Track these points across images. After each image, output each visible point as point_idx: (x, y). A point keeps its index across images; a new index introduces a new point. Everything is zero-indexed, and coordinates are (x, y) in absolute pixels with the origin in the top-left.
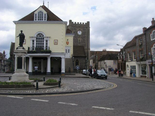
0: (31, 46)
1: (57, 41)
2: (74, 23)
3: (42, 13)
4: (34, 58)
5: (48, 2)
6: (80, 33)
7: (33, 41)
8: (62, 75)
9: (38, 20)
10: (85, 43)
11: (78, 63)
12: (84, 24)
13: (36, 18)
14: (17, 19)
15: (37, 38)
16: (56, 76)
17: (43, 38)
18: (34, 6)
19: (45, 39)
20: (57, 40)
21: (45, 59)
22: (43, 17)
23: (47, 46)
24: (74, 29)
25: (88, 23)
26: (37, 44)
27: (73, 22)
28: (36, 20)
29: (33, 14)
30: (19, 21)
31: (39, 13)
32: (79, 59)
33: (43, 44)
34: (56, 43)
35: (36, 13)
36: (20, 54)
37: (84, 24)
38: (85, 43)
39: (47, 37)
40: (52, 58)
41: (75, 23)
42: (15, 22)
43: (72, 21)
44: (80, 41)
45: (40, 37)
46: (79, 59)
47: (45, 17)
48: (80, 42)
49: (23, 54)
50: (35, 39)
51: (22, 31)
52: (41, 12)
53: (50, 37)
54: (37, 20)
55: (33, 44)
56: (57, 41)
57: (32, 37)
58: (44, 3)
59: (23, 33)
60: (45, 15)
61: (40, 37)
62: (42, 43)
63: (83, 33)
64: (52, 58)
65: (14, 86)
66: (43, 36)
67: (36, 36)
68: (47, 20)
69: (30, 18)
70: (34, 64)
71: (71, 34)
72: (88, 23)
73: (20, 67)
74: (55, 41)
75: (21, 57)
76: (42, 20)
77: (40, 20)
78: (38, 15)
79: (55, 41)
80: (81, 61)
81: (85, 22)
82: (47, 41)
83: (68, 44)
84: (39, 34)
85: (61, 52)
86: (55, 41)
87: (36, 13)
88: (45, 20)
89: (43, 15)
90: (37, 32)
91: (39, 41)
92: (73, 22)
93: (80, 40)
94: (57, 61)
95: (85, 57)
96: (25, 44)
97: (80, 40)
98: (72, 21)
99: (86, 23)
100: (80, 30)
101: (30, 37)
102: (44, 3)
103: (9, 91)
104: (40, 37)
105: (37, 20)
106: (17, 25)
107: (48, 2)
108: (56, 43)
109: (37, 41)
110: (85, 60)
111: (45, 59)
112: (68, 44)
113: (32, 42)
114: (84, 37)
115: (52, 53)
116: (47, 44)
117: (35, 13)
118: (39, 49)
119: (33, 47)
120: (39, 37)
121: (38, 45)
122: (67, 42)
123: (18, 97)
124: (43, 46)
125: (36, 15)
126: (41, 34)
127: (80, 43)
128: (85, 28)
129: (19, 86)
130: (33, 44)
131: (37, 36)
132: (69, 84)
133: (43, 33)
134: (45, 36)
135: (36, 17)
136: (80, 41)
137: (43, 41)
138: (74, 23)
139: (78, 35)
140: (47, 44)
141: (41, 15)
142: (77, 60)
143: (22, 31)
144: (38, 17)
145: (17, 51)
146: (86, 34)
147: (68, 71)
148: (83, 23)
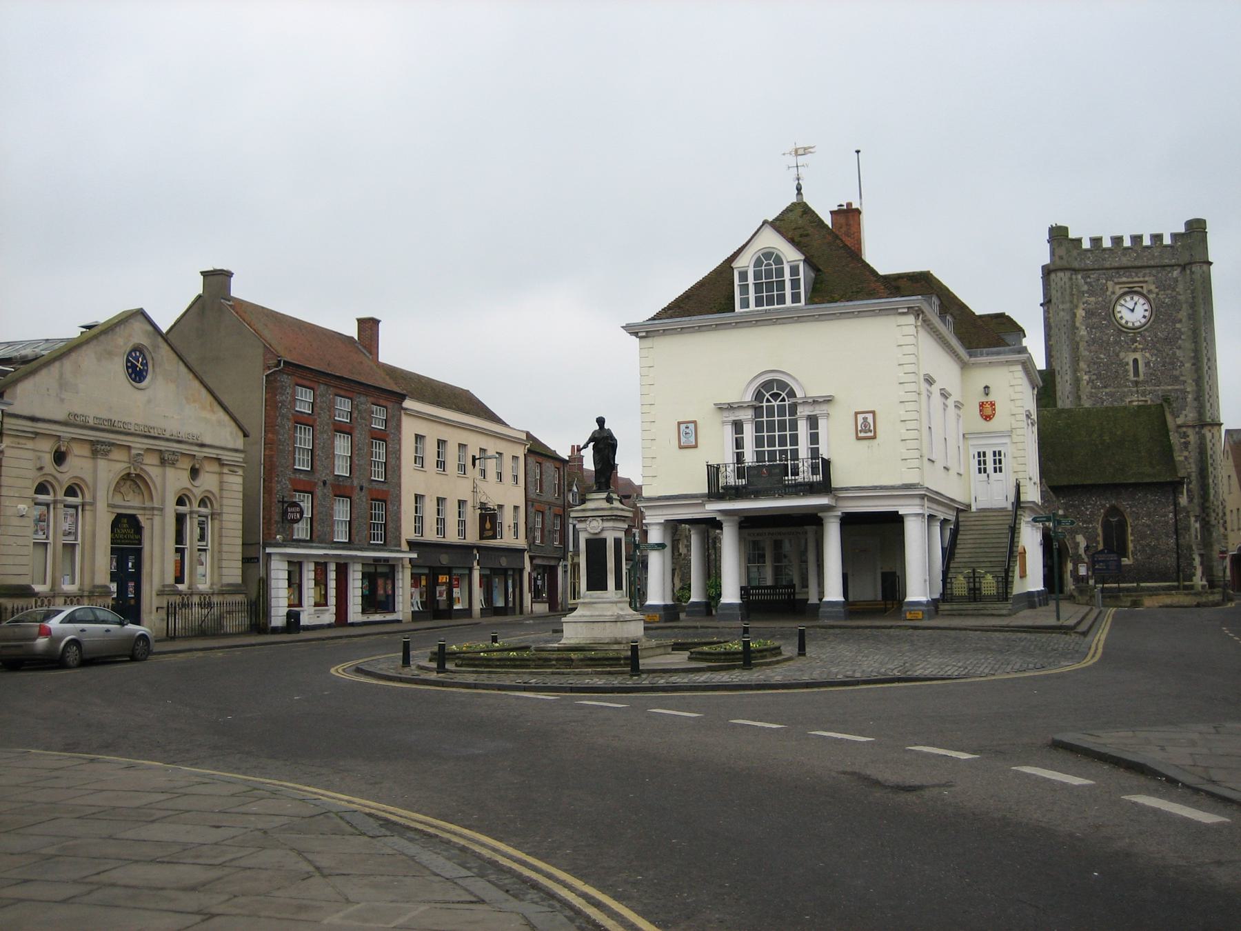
0: (725, 456)
1: (870, 420)
2: (1086, 245)
3: (779, 261)
4: (748, 523)
5: (858, 152)
6: (1133, 312)
7: (738, 426)
8: (909, 616)
9: (759, 302)
10: (1176, 379)
11: (1124, 532)
12: (1167, 241)
13: (746, 301)
14: (645, 312)
15: (758, 410)
16: (877, 623)
17: (793, 409)
18: (728, 221)
19: (803, 411)
20: (873, 413)
21: (813, 520)
22: (781, 285)
23: (815, 453)
24: (1085, 288)
25: (1197, 228)
26: (759, 442)
27: (1079, 241)
28: (745, 303)
29: (725, 269)
30: (658, 317)
31: (758, 263)
32: (1125, 505)
33: (794, 439)
34: (866, 431)
35: (745, 262)
36: (594, 526)
37: (1167, 241)
38: (1176, 379)
39: (815, 402)
40: (850, 522)
41: (1096, 241)
42: (633, 330)
43: (1072, 235)
44: (1136, 373)
45: (774, 402)
46: (1125, 505)
47: (796, 284)
48: (1142, 377)
49: (610, 524)
50: (747, 416)
51: (601, 421)
52: (768, 255)
53: (828, 400)
54: (752, 306)
55: (739, 444)
56: (870, 417)
57: (730, 407)
58: (799, 189)
59: (606, 426)
60: (794, 270)
61: (774, 402)
62: (788, 433)
63: (1159, 313)
64: (850, 522)
65: (550, 660)
66: (792, 394)
67: (748, 397)
68: (810, 301)
69: (709, 301)
70: (752, 555)
71: (1004, 353)
72: (1197, 228)
73: (597, 582)
74: (860, 421)
75: (604, 535)
76: (782, 300)
77: (770, 301)
78: (757, 275)
79: (860, 421)
80: (1144, 520)
81: (1172, 226)
82: (813, 422)
83: (987, 418)
84: (767, 385)
85: (898, 482)
86: (860, 417)
87: (745, 262)
88: (796, 298)
89: (780, 273)
90: (756, 377)
91: (771, 427)
92: (1079, 241)
93: (1136, 361)
94: (875, 534)
95: (1175, 486)
96: (696, 446)
97: (1136, 361)
98: (1072, 235)
99: (1175, 236)
100: (1131, 292)
101: (721, 408)
102: (799, 189)
103: (526, 678)
104: (775, 403)
105: (752, 306)
106: (648, 343)
107: (858, 152)
108: (866, 431)
109: (759, 427)
110: (1176, 504)
111: (813, 520)
112: (987, 418)
113: (729, 431)
114: (1171, 340)
115: (837, 489)
116: (814, 438)
117: (739, 264)
118: (767, 475)
119: (739, 457)
120: (768, 401)
121: (789, 447)
122: (982, 405)
123: (541, 696)
124: (795, 453)
125: (743, 276)
126: (783, 385)
127: (1136, 383)
128: (1176, 273)
129: (569, 662)
130: (739, 444)
131: (759, 396)
132: (832, 657)
133: (794, 378)
134: (799, 394)
135: (744, 289)
136: (1136, 373)
137: (794, 426)
138: (1086, 245)
139: (1122, 329)
140: (814, 438)
141: (769, 274)
142: (1114, 510)
143: (601, 421)
144: (758, 288)
145: (584, 510)
146: (1183, 314)
147: (965, 592)
148: (1157, 238)
